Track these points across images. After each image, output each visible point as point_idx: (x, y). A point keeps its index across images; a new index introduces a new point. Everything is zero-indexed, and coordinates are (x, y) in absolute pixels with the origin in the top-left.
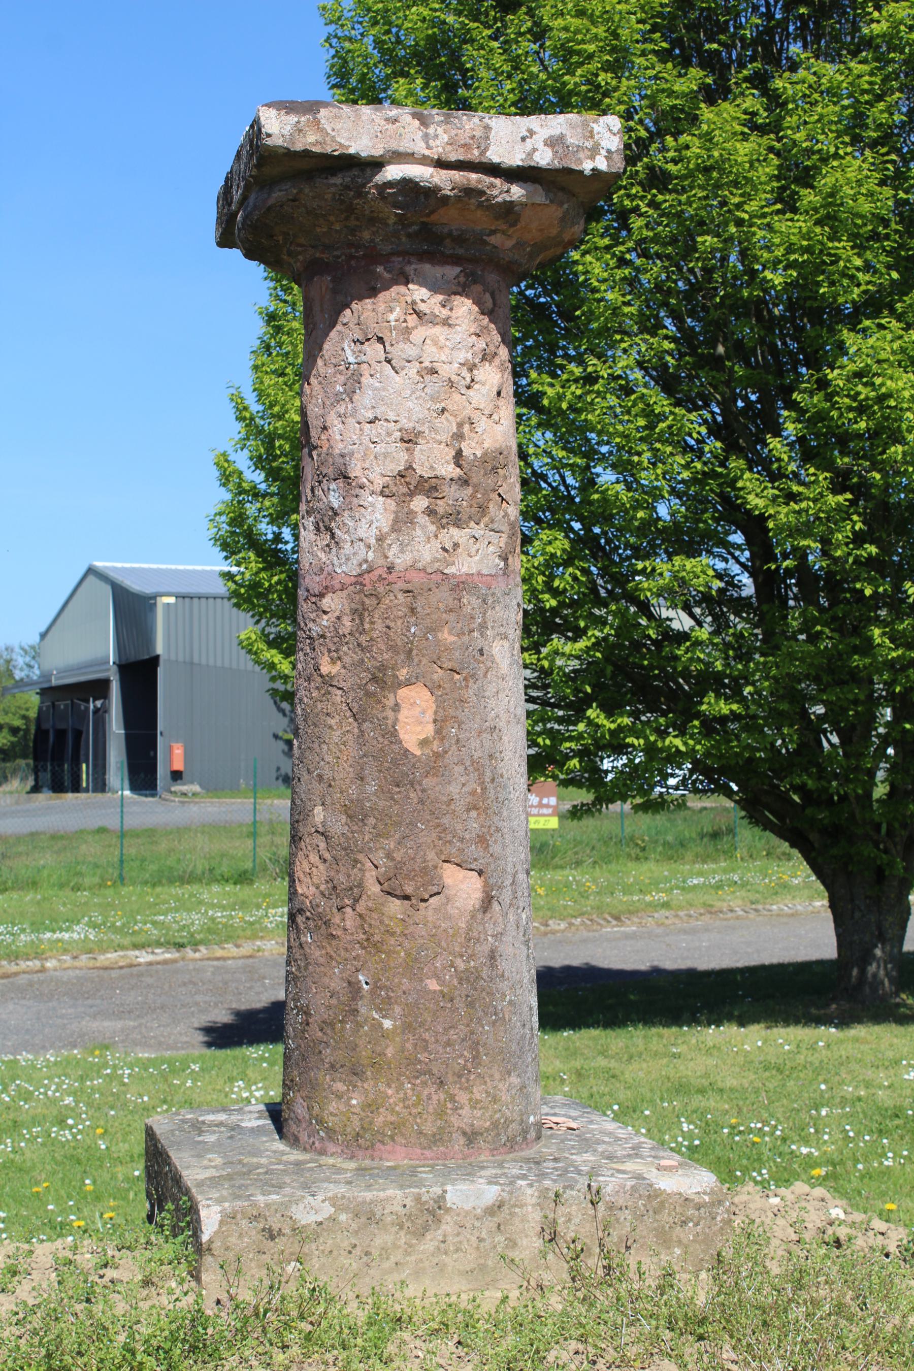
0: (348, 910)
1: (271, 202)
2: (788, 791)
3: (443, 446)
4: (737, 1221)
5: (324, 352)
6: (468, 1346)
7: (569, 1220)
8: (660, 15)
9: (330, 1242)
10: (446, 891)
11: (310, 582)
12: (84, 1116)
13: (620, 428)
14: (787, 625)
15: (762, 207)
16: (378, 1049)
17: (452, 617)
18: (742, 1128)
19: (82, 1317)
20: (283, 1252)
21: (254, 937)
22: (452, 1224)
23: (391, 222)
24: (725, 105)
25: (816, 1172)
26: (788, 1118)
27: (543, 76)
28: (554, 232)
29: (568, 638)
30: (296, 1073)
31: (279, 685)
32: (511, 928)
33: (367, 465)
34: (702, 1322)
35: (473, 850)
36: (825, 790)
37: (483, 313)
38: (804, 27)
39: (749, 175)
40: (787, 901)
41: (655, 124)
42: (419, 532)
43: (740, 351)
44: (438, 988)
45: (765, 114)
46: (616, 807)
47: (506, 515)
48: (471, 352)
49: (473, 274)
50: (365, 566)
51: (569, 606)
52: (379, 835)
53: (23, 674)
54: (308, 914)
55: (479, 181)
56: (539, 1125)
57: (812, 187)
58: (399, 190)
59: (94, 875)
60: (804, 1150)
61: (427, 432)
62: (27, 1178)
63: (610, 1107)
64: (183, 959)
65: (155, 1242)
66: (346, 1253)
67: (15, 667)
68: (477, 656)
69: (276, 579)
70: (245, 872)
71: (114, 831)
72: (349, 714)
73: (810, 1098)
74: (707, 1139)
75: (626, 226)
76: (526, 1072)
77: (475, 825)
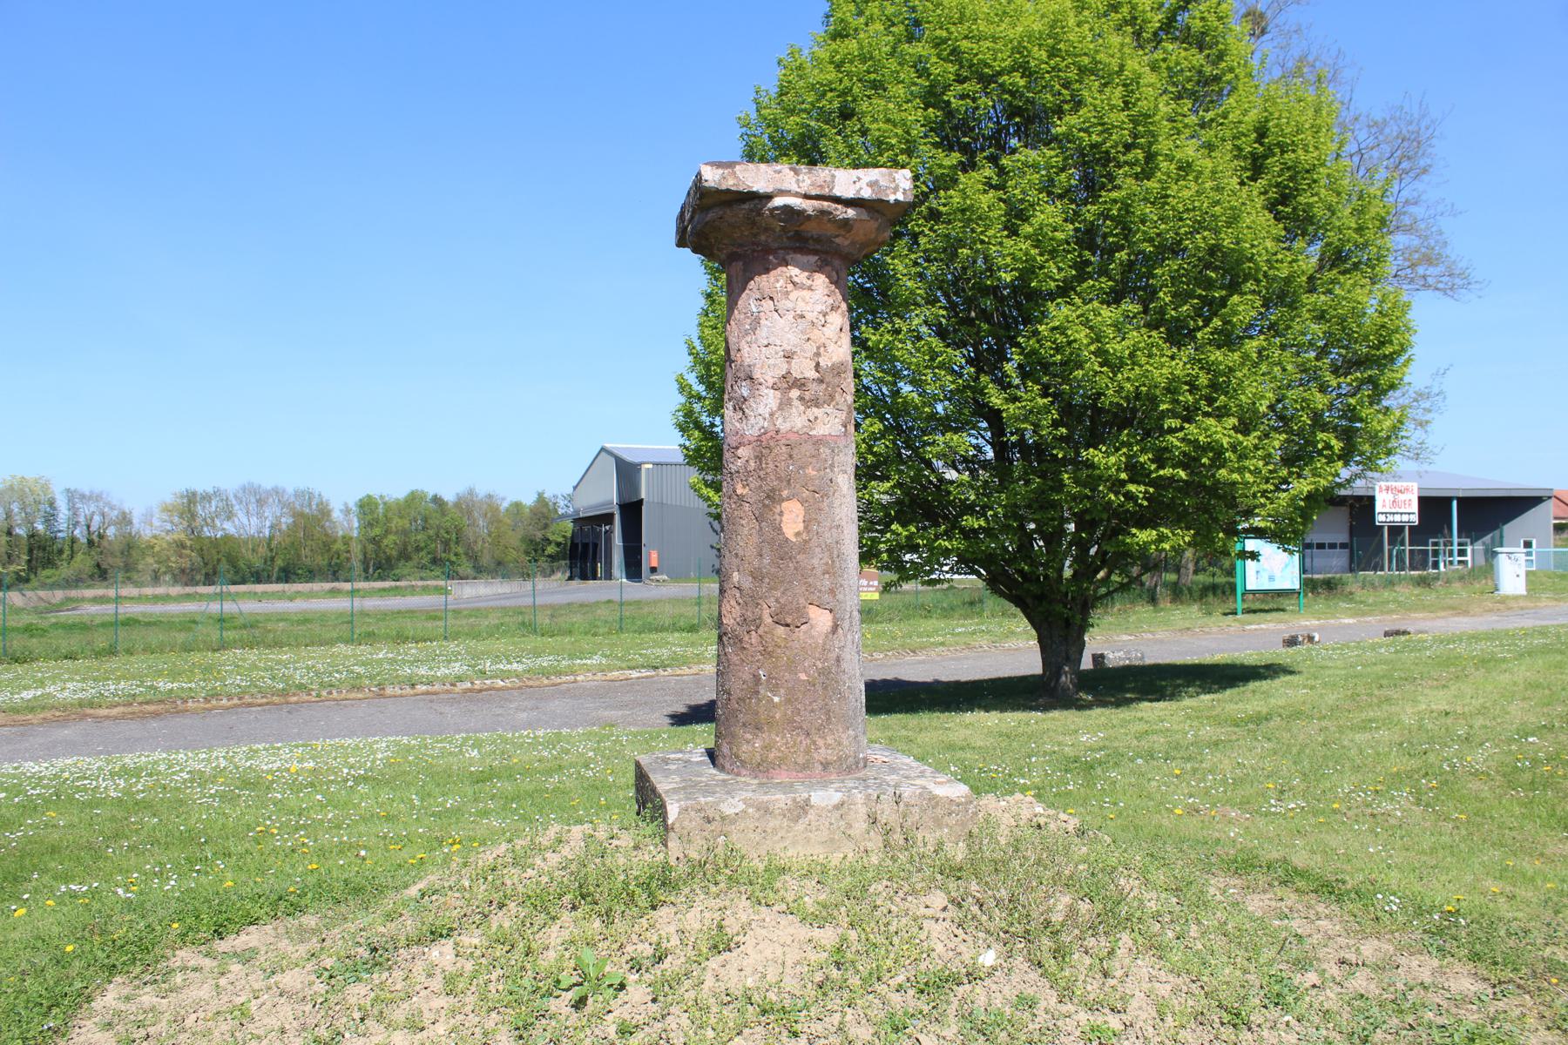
21: (699, 663)
31: (712, 510)
32: (849, 643)
43: (985, 315)
75: (916, 243)
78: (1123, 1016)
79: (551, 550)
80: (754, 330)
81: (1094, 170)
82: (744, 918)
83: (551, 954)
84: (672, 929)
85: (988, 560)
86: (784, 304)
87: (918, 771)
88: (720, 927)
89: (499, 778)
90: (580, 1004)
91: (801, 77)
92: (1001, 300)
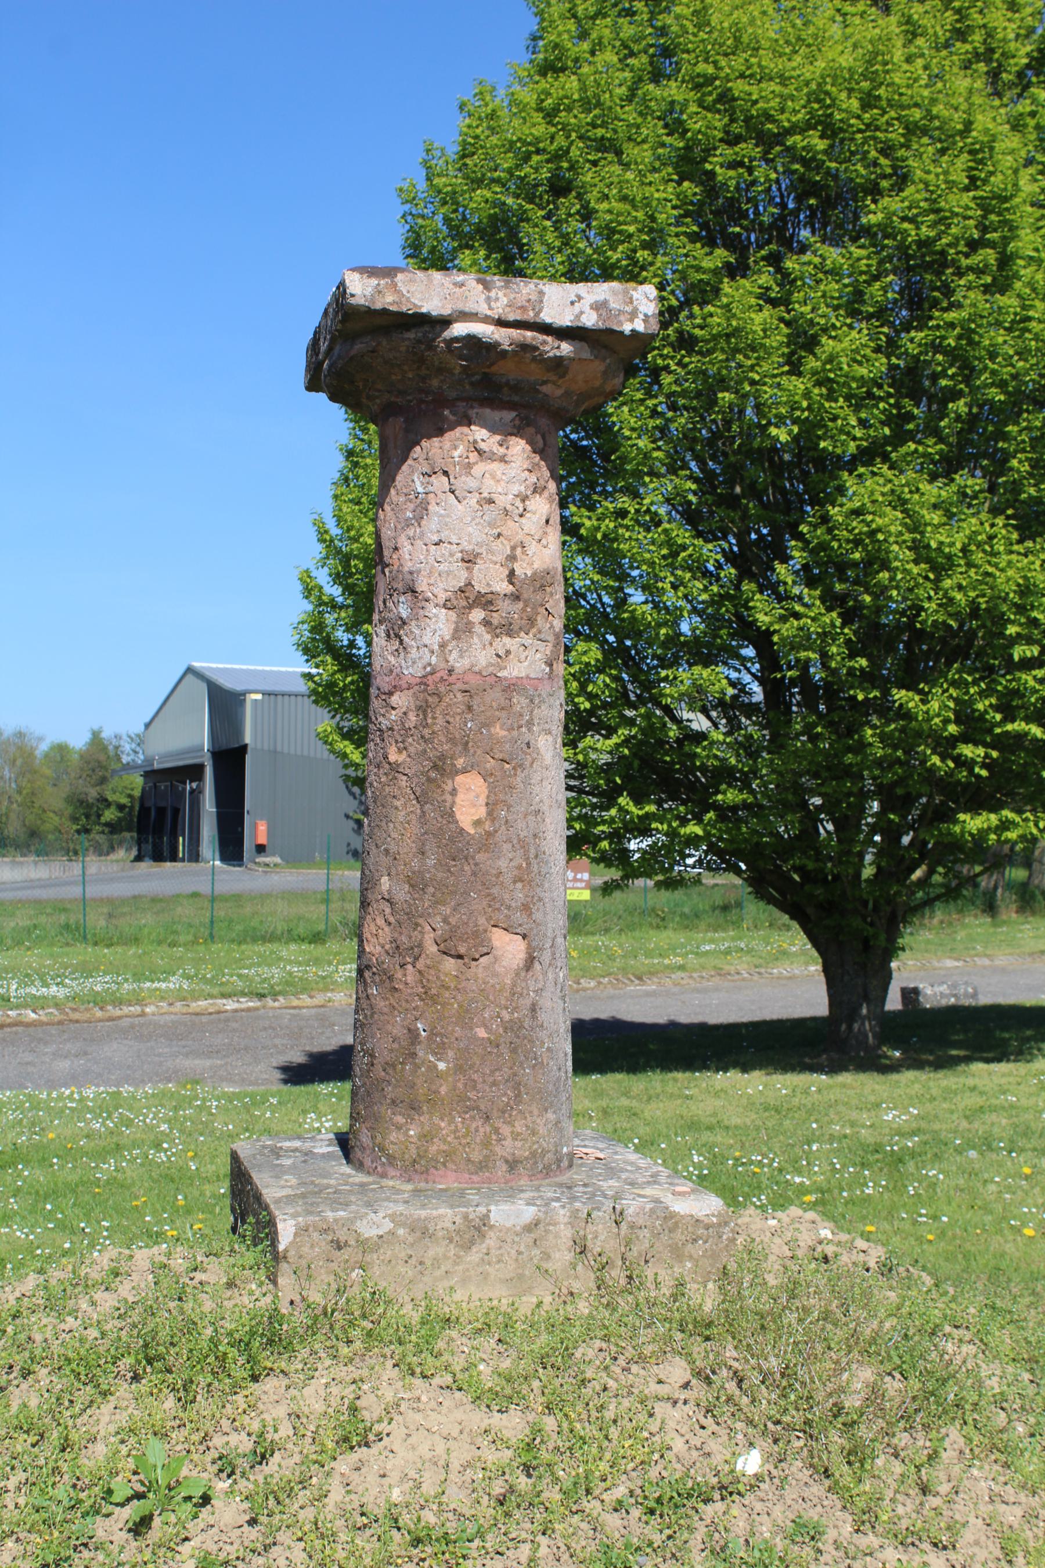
0: (409, 967)
1: (352, 353)
2: (789, 870)
4: (740, 1240)
7: (596, 1237)
8: (692, 203)
9: (389, 1252)
11: (381, 681)
17: (503, 714)
19: (175, 1313)
21: (326, 989)
23: (457, 371)
24: (743, 281)
27: (589, 251)
28: (597, 383)
31: (351, 772)
33: (432, 581)
34: (709, 1325)
35: (518, 917)
37: (535, 452)
42: (476, 640)
43: (753, 491)
46: (640, 882)
47: (552, 627)
52: (437, 903)
53: (129, 759)
55: (534, 338)
56: (571, 1155)
57: (815, 355)
60: (798, 1180)
62: (127, 1193)
63: (631, 1140)
64: (264, 1007)
69: (349, 679)
70: (319, 933)
72: (412, 797)
75: (656, 381)
78: (952, 1555)
79: (110, 815)
81: (922, 277)
82: (389, 1395)
83: (100, 1449)
84: (281, 1411)
85: (754, 853)
86: (464, 482)
87: (646, 1172)
88: (354, 1410)
89: (27, 1163)
90: (140, 1527)
91: (493, 130)
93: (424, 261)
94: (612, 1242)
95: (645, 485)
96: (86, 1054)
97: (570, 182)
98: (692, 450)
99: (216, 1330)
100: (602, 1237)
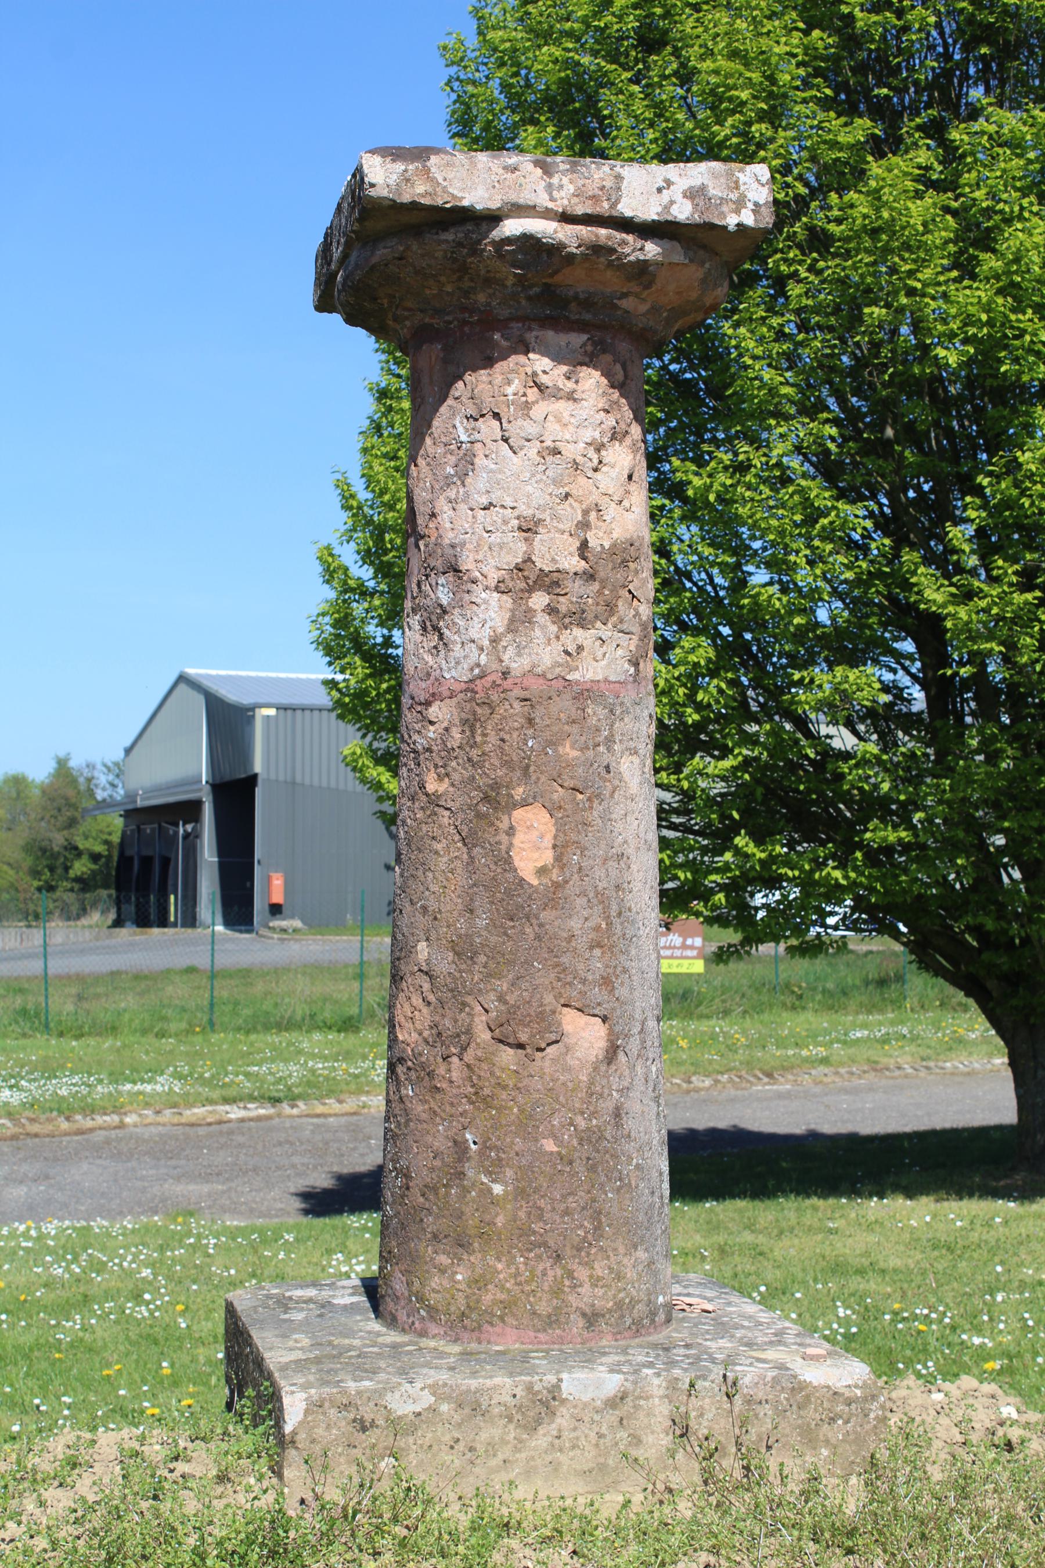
0: (455, 1060)
1: (374, 260)
2: (963, 932)
3: (566, 536)
4: (894, 1420)
5: (433, 429)
6: (584, 1556)
7: (702, 1415)
8: (823, 59)
9: (429, 1435)
10: (565, 1039)
11: (417, 688)
12: (163, 1290)
13: (774, 523)
14: (963, 743)
15: (938, 273)
16: (487, 1218)
17: (575, 729)
18: (906, 1315)
19: (148, 1516)
20: (374, 1446)
21: (360, 1091)
22: (568, 1417)
23: (509, 283)
24: (895, 160)
25: (989, 1366)
26: (959, 1304)
27: (690, 125)
28: (694, 295)
29: (713, 756)
30: (394, 1243)
31: (387, 807)
32: (639, 1082)
33: (480, 557)
34: (851, 1534)
35: (597, 993)
36: (1005, 932)
37: (612, 387)
38: (987, 68)
39: (924, 239)
40: (962, 1058)
41: (817, 179)
42: (538, 632)
43: (911, 434)
44: (556, 1149)
45: (941, 168)
46: (766, 949)
47: (637, 614)
48: (599, 430)
49: (602, 342)
50: (477, 671)
51: (716, 721)
52: (490, 975)
53: (105, 794)
54: (410, 1063)
55: (609, 238)
56: (670, 1307)
57: (994, 251)
58: (518, 247)
59: (181, 1020)
60: (977, 1341)
61: (548, 519)
62: (97, 1359)
63: (756, 1288)
64: (279, 1115)
65: (233, 1433)
66: (447, 1448)
67: (96, 786)
68: (603, 773)
69: (384, 686)
70: (350, 1018)
71: (205, 971)
72: (457, 837)
73: (984, 1281)
74: (866, 1326)
76: (654, 1246)
77: (599, 965)
79: (81, 867)
80: (463, 476)
85: (914, 909)
86: (520, 428)
87: (767, 1330)
92: (943, 404)
93: (476, 140)
94: (723, 1422)
95: (769, 429)
96: (47, 1177)
97: (666, 32)
98: (830, 383)
99: (202, 1538)
100: (709, 1416)
